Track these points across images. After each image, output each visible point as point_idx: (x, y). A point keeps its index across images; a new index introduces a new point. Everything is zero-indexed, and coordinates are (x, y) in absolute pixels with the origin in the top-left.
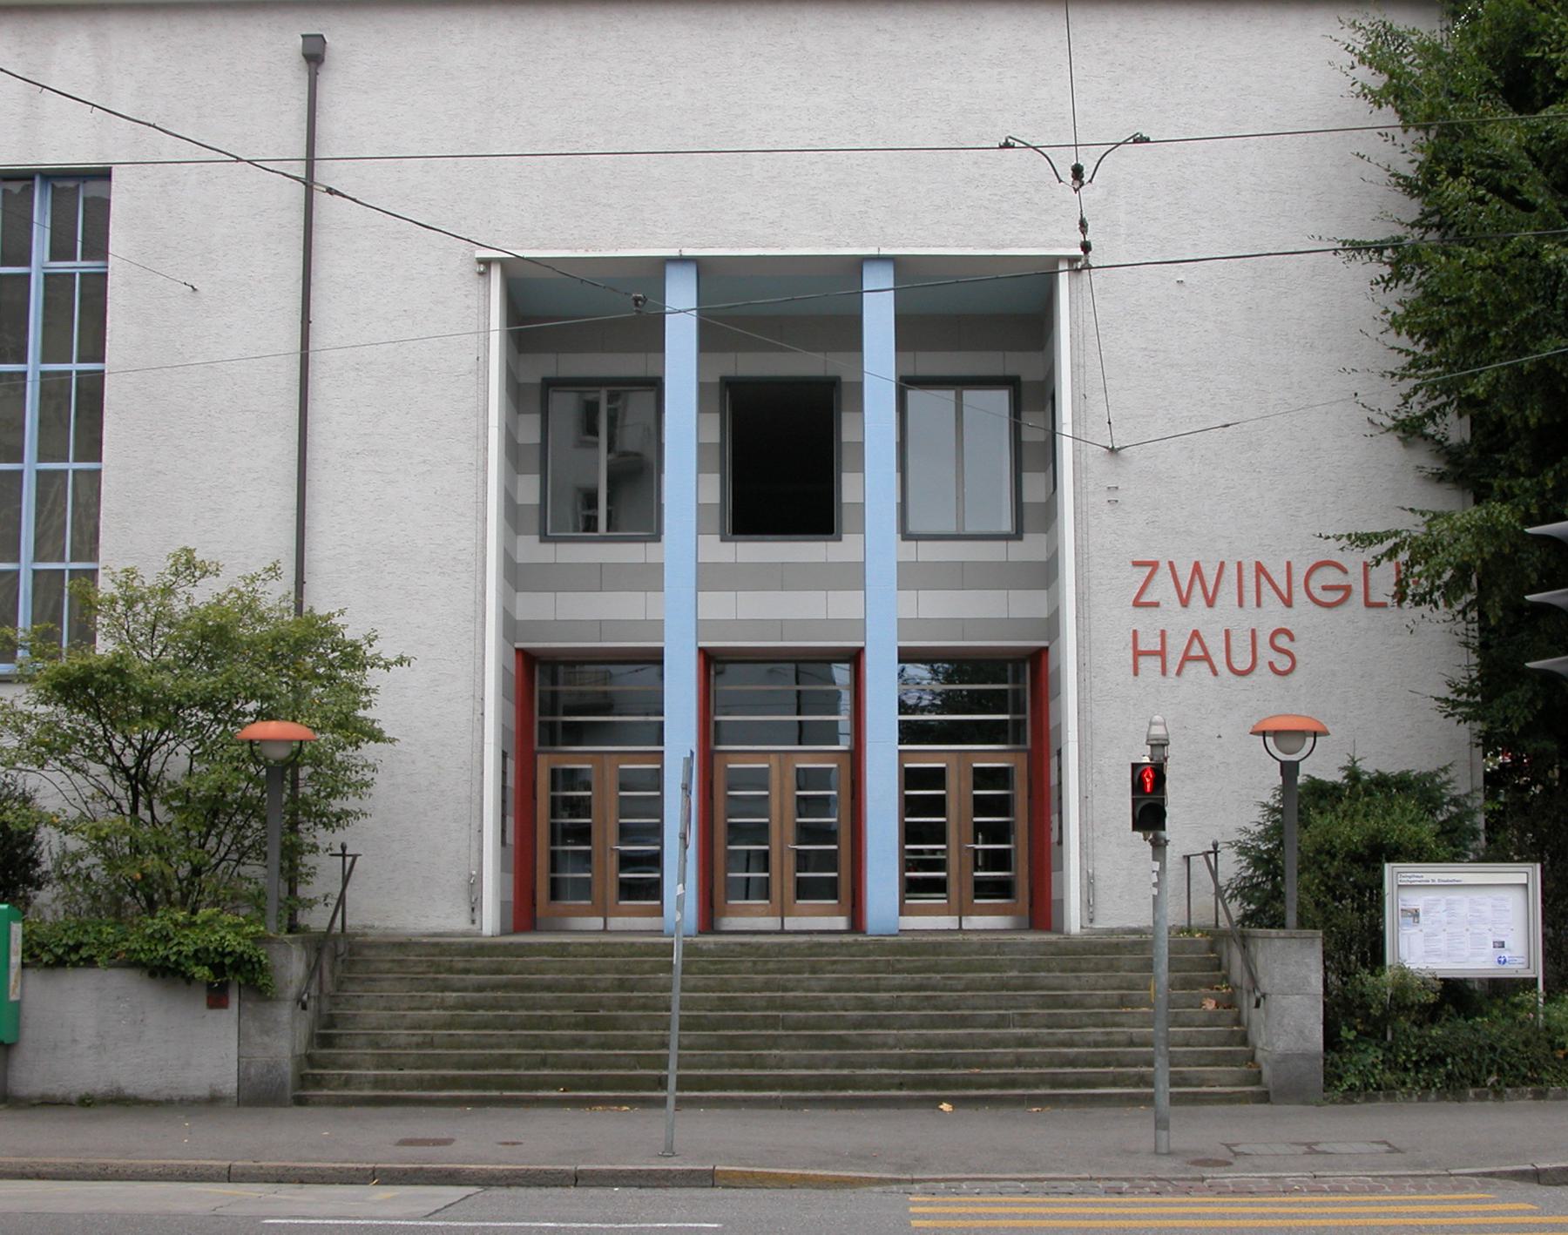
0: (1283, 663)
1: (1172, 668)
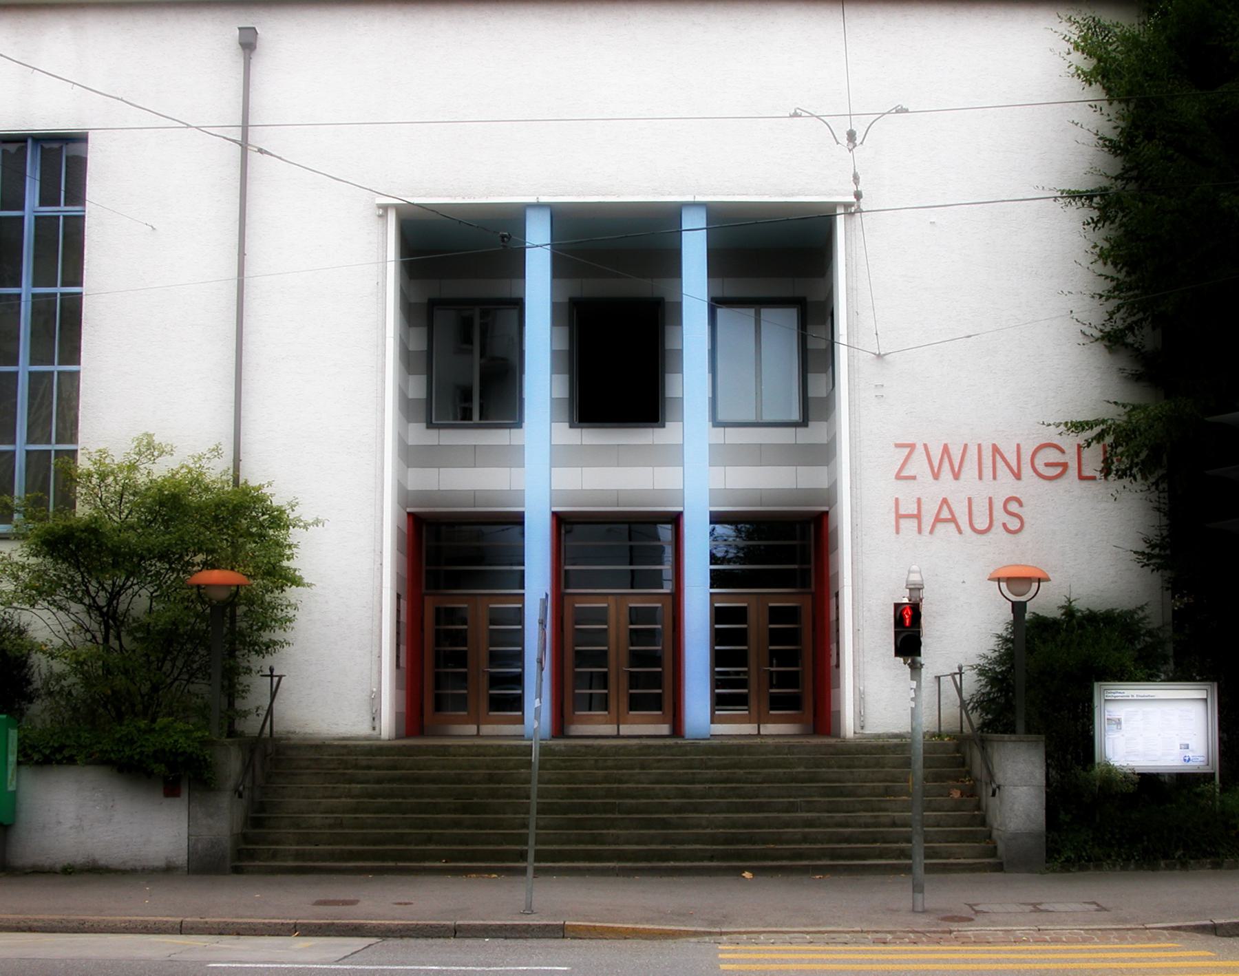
0: (1014, 524)
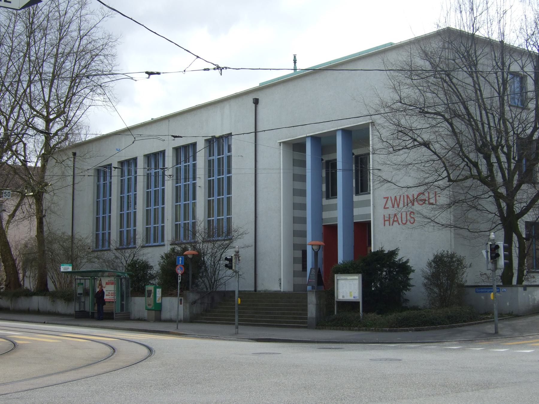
0: (412, 221)
1: (391, 224)
